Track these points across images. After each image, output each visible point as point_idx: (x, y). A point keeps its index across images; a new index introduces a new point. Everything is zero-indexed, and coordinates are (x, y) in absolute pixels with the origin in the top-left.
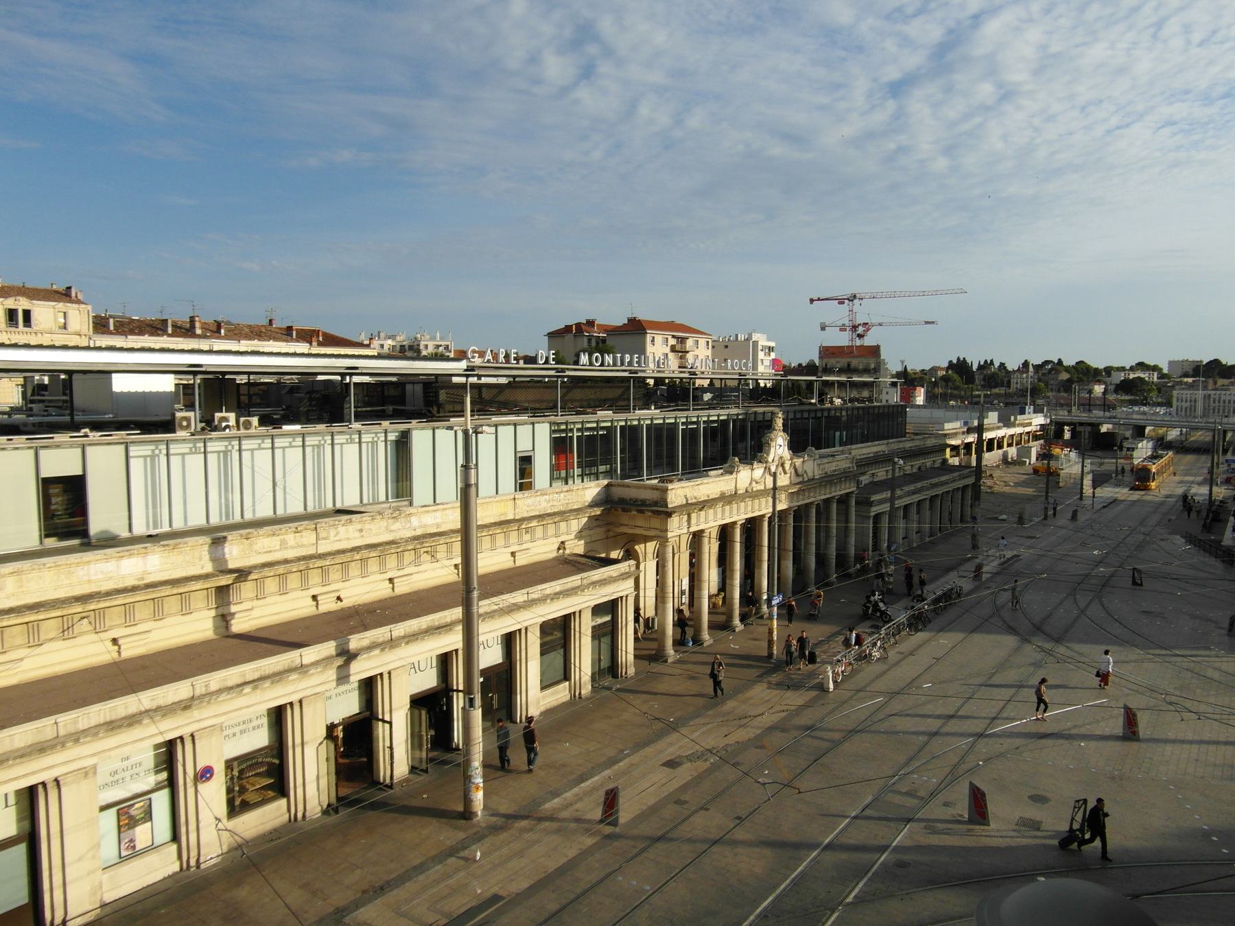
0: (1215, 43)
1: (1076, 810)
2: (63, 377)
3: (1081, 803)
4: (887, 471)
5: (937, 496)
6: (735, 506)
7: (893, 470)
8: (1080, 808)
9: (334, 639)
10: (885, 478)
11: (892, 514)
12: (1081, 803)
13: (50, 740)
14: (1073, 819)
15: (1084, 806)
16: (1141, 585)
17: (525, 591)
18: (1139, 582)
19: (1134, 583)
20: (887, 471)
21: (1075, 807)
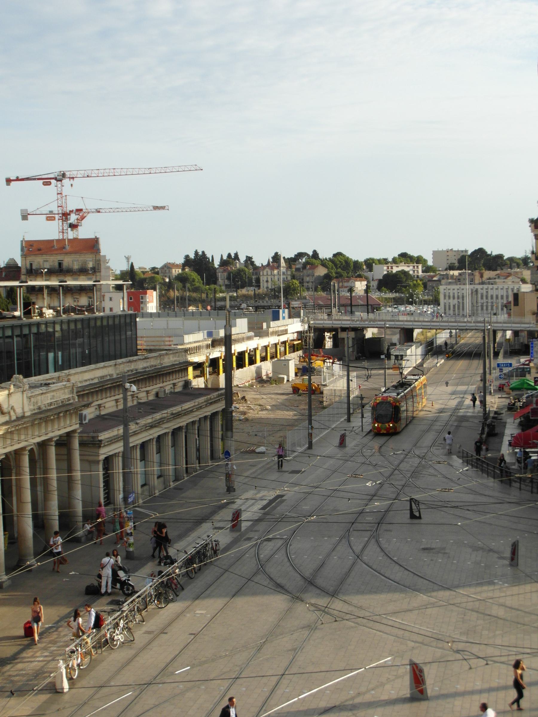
7: (125, 399)
10: (114, 409)
16: (420, 517)
18: (417, 514)
20: (117, 401)
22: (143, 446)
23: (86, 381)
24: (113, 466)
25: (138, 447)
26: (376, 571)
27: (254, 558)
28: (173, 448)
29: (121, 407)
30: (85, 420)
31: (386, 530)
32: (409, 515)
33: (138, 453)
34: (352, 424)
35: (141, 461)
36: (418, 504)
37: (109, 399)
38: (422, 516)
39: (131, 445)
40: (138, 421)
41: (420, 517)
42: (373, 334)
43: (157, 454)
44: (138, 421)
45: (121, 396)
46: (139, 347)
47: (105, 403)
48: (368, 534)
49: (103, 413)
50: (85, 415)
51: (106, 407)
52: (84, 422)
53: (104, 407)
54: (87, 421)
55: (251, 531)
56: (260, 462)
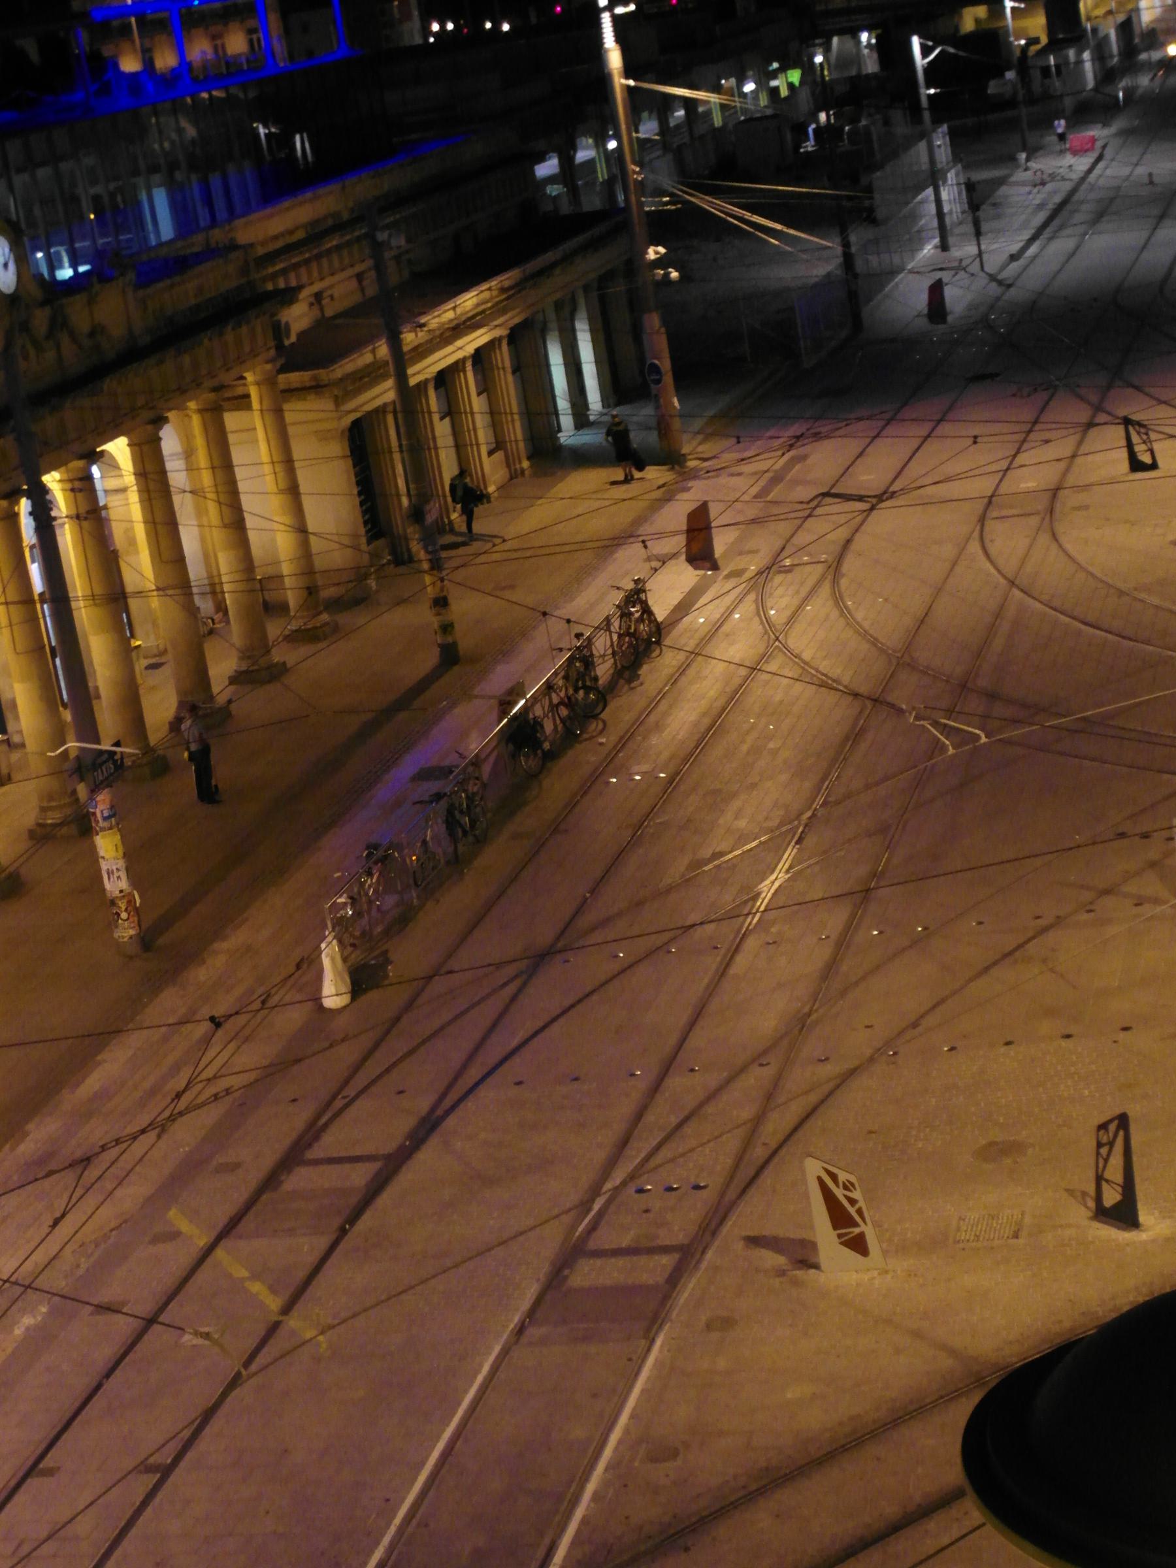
0: (1071, 180)
1: (1104, 1151)
2: (775, 65)
3: (1112, 1127)
4: (359, 277)
5: (457, 367)
6: (229, 336)
7: (379, 267)
8: (1111, 1144)
9: (123, 434)
10: (357, 298)
11: (409, 397)
12: (1112, 1127)
13: (471, 310)
14: (1099, 1179)
15: (1121, 1133)
16: (1154, 466)
17: (451, 305)
18: (1146, 459)
19: (1136, 465)
20: (359, 277)
21: (1099, 1145)
22: (445, 379)
23: (275, 238)
24: (456, 393)
25: (469, 366)
26: (1062, 613)
27: (757, 619)
28: (447, 420)
29: (372, 290)
30: (288, 337)
31: (1079, 508)
32: (1125, 466)
33: (433, 400)
34: (956, 253)
35: (514, 372)
36: (1147, 434)
37: (337, 278)
38: (1160, 463)
39: (412, 382)
40: (423, 320)
41: (1154, 466)
42: (977, 21)
43: (479, 394)
44: (423, 320)
45: (370, 263)
46: (224, 71)
47: (331, 287)
48: (1034, 521)
49: (329, 313)
50: (287, 324)
51: (336, 295)
52: (287, 343)
53: (332, 297)
54: (293, 338)
55: (741, 553)
56: (850, 1233)
